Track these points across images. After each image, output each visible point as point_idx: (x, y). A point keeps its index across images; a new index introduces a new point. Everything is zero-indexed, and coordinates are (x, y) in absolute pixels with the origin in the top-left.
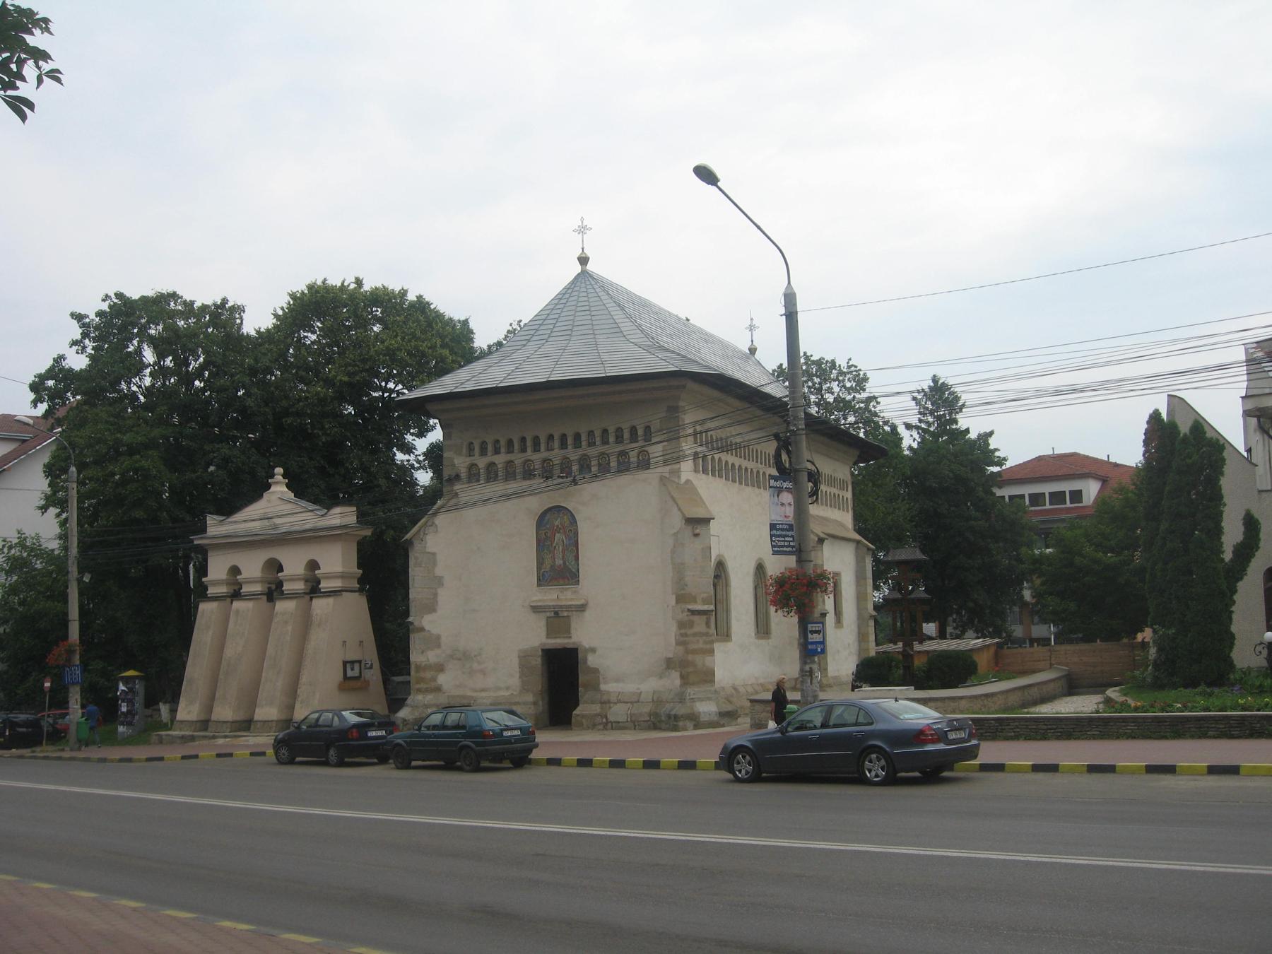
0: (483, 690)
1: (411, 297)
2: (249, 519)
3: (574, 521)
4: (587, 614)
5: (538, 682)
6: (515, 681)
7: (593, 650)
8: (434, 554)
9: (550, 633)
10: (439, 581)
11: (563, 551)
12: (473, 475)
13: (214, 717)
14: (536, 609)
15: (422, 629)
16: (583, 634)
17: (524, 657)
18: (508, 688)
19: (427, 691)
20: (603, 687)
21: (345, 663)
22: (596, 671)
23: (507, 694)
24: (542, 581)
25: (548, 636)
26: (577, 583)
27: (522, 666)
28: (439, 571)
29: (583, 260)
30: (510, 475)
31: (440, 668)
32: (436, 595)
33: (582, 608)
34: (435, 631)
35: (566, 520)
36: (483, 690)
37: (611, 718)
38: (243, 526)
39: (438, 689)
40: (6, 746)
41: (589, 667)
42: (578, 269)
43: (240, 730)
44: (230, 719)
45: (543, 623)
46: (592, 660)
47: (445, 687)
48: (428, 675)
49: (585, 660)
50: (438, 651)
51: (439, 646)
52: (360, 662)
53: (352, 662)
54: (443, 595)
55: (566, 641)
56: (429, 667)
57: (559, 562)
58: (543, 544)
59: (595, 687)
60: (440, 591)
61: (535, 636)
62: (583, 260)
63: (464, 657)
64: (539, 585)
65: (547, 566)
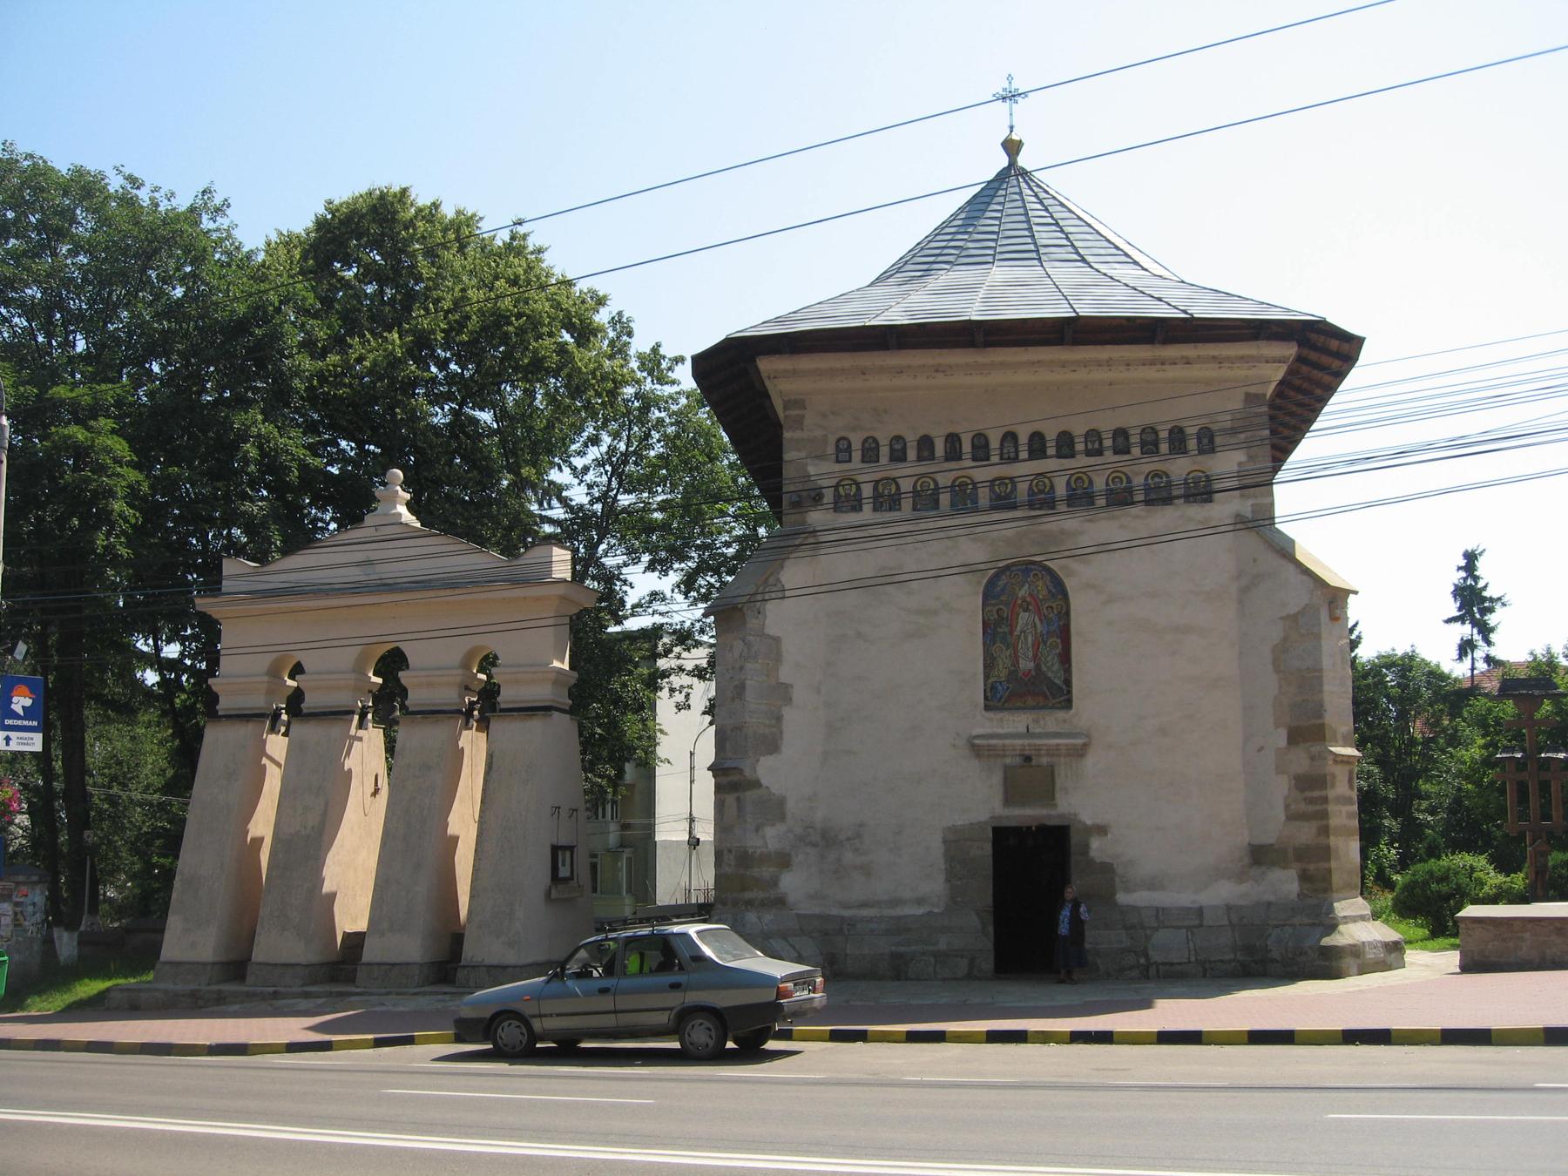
0: (864, 905)
1: (448, 211)
2: (333, 556)
3: (1059, 590)
4: (1090, 762)
5: (983, 892)
6: (934, 886)
7: (1102, 830)
8: (777, 640)
9: (1012, 794)
10: (783, 693)
11: (1036, 646)
12: (848, 501)
13: (258, 955)
14: (978, 749)
15: (756, 784)
16: (1080, 800)
17: (955, 842)
18: (920, 901)
19: (765, 904)
20: (1122, 898)
21: (555, 849)
22: (1107, 869)
23: (920, 911)
24: (995, 700)
25: (1008, 801)
26: (1068, 704)
27: (950, 857)
28: (785, 674)
29: (1012, 147)
30: (926, 500)
31: (784, 861)
32: (779, 719)
33: (1080, 752)
34: (776, 789)
35: (1042, 587)
36: (864, 905)
37: (1156, 957)
38: (283, 577)
39: (780, 902)
40: (13, 1001)
41: (1091, 862)
42: (1004, 161)
43: (314, 983)
44: (302, 960)
45: (997, 779)
46: (1098, 848)
47: (791, 898)
48: (766, 872)
49: (1086, 848)
50: (781, 828)
51: (783, 818)
52: (571, 848)
53: (564, 848)
54: (793, 719)
55: (1044, 812)
56: (765, 859)
57: (1026, 665)
58: (995, 630)
59: (1108, 898)
60: (787, 712)
61: (980, 801)
62: (1012, 147)
63: (826, 840)
64: (987, 708)
65: (1001, 672)
